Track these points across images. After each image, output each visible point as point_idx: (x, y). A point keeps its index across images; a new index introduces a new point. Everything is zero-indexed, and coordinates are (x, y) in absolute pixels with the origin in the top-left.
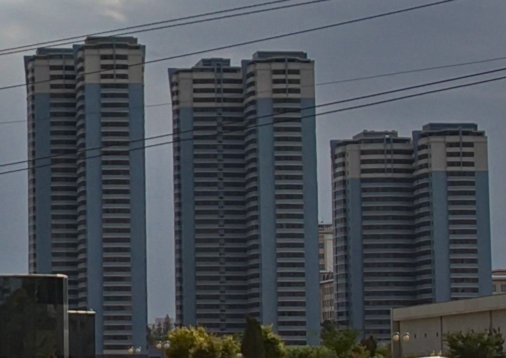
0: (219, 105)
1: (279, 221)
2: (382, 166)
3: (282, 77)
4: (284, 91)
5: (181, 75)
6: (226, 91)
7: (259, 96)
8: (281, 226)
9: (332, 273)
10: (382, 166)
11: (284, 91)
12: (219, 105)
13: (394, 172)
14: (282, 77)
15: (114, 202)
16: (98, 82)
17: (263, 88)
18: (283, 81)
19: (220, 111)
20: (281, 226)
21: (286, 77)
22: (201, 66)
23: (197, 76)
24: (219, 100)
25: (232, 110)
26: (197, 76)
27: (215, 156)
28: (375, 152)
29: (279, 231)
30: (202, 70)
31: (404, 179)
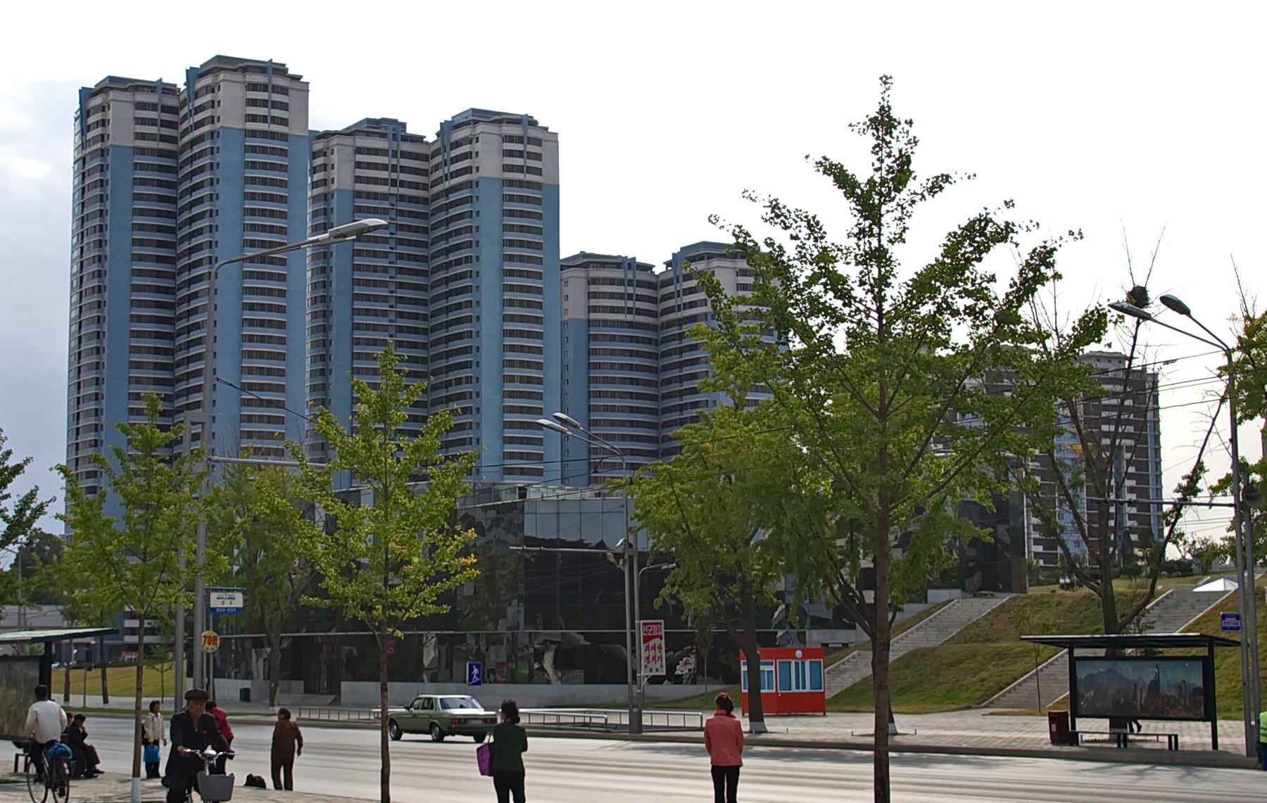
0: (394, 190)
1: (508, 372)
2: (621, 303)
3: (519, 147)
4: (520, 169)
5: (334, 141)
6: (404, 169)
7: (484, 173)
8: (511, 379)
9: (991, 305)
10: (621, 303)
11: (520, 169)
12: (394, 190)
13: (637, 314)
14: (519, 147)
15: (262, 323)
16: (240, 127)
17: (489, 164)
18: (520, 154)
19: (393, 200)
20: (511, 379)
21: (525, 147)
22: (364, 128)
23: (363, 142)
24: (394, 183)
25: (412, 199)
26: (363, 142)
27: (385, 270)
28: (612, 282)
29: (509, 387)
30: (368, 134)
31: (649, 324)
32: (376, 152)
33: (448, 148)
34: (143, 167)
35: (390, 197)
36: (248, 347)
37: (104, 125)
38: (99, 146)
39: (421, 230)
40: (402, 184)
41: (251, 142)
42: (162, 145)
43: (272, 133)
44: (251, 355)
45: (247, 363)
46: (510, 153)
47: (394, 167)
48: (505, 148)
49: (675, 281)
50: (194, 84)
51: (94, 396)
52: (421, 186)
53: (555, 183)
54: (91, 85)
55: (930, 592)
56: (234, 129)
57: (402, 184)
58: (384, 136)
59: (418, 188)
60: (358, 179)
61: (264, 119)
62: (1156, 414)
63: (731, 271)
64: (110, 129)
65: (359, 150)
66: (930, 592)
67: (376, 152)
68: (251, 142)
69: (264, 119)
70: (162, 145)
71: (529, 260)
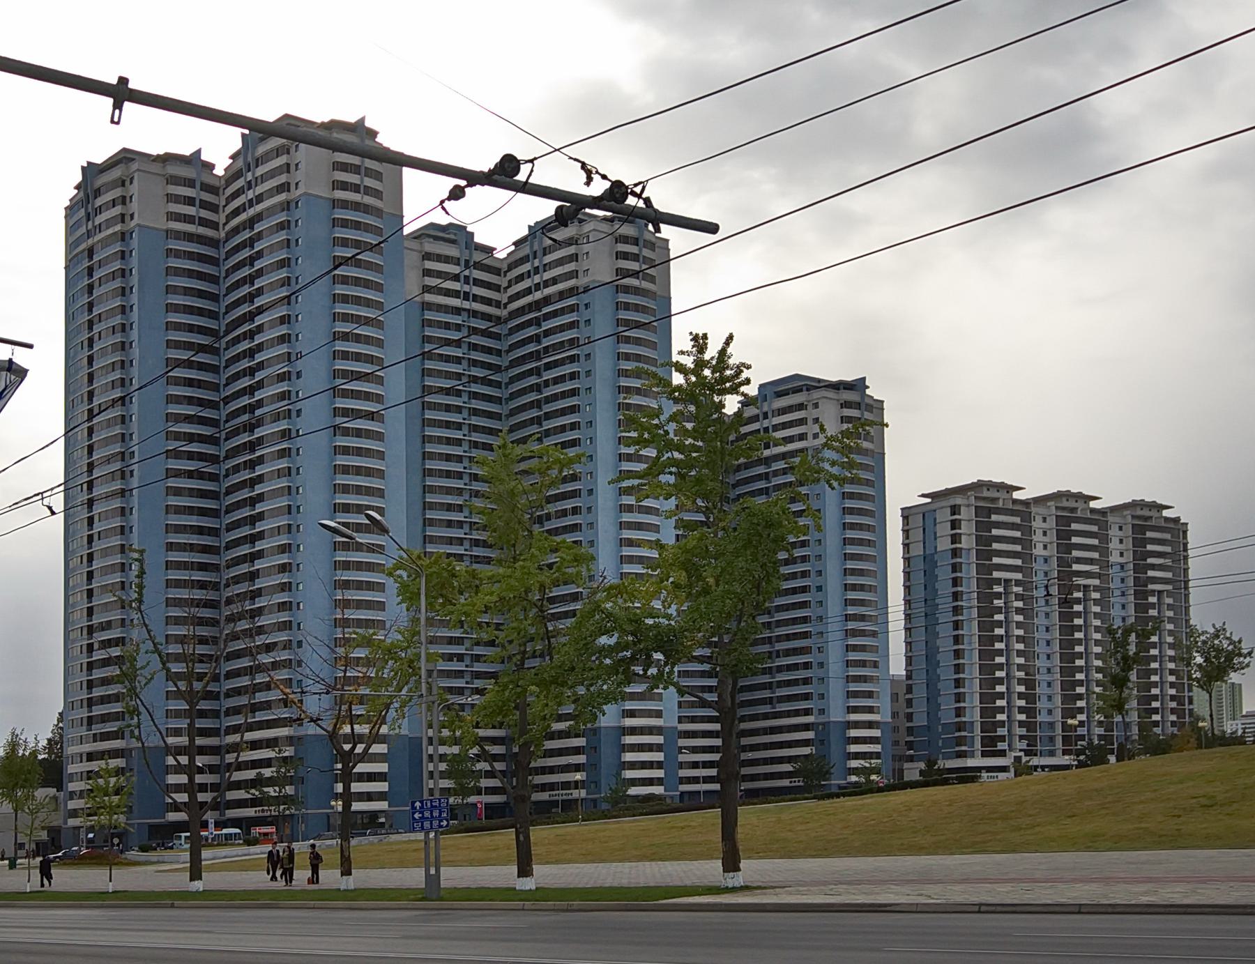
0: (466, 305)
12: (466, 305)
32: (447, 259)
33: (539, 254)
34: (178, 254)
35: (463, 313)
36: (342, 460)
37: (124, 203)
38: (118, 228)
39: (494, 352)
40: (476, 298)
41: (341, 214)
42: (202, 230)
43: (366, 206)
44: (346, 470)
45: (341, 480)
46: (625, 256)
47: (467, 279)
48: (619, 249)
49: (761, 418)
50: (255, 148)
51: (119, 530)
52: (494, 303)
53: (666, 295)
54: (99, 159)
55: (386, 752)
56: (321, 197)
57: (476, 298)
58: (453, 242)
59: (490, 305)
60: (427, 289)
61: (356, 188)
62: (1186, 563)
63: (835, 402)
64: (134, 206)
65: (427, 256)
66: (386, 752)
67: (447, 259)
68: (341, 214)
69: (356, 188)
70: (202, 230)
71: (369, 472)
